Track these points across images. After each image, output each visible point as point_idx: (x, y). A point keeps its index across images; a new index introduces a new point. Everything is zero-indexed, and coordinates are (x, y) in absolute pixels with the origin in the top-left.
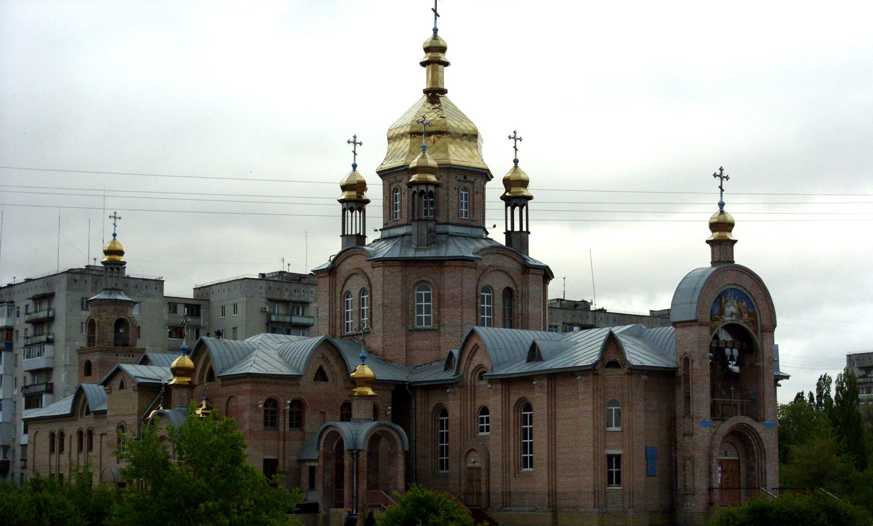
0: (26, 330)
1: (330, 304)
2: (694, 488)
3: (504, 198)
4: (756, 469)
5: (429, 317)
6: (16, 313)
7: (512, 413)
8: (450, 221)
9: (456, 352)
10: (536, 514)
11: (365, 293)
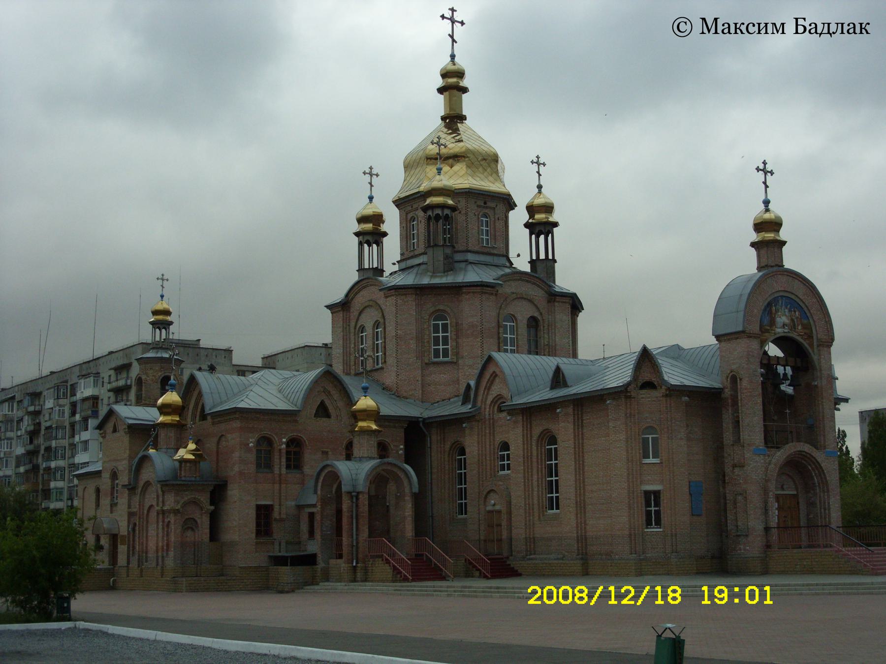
0: (109, 398)
1: (343, 340)
2: (748, 528)
3: (527, 225)
4: (818, 504)
5: (447, 349)
6: (101, 383)
7: (534, 448)
8: (469, 249)
9: (472, 383)
10: (564, 562)
11: (379, 327)
